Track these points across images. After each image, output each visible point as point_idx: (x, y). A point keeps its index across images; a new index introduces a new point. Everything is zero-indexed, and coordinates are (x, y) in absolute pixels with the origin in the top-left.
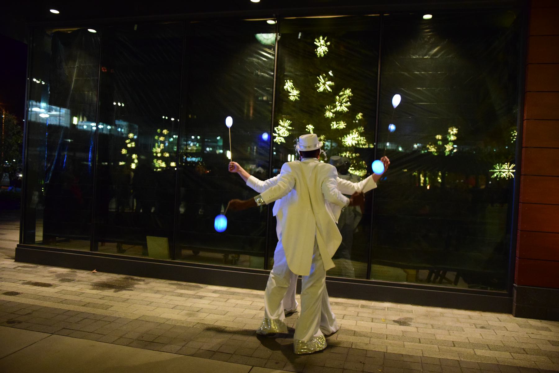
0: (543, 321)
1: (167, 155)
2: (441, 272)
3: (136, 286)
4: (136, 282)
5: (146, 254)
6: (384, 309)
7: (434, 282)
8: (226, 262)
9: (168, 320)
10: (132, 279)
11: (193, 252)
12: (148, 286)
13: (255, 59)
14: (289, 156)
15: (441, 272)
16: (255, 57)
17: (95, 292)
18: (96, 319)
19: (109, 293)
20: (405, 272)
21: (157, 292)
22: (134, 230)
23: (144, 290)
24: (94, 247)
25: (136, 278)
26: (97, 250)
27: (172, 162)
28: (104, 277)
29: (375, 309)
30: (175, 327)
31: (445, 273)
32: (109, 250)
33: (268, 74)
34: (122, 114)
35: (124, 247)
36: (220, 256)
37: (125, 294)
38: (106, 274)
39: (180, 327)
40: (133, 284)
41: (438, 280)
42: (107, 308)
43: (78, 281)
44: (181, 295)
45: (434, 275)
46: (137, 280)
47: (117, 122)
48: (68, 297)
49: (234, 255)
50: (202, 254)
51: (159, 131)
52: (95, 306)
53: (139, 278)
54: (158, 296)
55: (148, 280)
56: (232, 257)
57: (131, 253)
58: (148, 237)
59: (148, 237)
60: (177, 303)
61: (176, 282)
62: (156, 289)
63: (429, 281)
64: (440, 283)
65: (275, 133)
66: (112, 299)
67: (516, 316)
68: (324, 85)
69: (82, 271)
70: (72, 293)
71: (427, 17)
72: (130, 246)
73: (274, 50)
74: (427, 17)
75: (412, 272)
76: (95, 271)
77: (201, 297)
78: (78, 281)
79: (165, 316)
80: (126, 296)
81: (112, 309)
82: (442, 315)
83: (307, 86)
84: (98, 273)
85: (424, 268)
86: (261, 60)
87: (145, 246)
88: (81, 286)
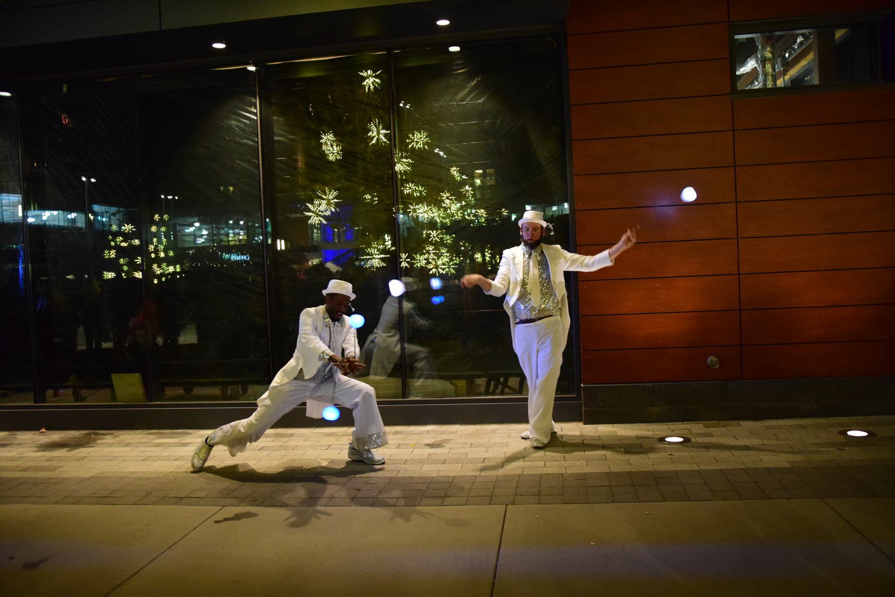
0: (615, 425)
1: (171, 254)
2: (502, 380)
3: (99, 442)
4: (101, 437)
5: (114, 399)
6: (428, 432)
7: (494, 394)
8: (225, 398)
9: (132, 473)
10: (95, 434)
11: (184, 389)
12: (118, 439)
13: (234, 123)
14: (283, 248)
15: (502, 380)
16: (233, 119)
17: (40, 454)
18: (36, 482)
19: (62, 453)
20: (451, 383)
21: (128, 444)
22: (97, 371)
23: (110, 445)
24: (40, 397)
25: (102, 432)
26: (45, 402)
27: (528, 204)
28: (56, 436)
29: (411, 433)
30: (140, 479)
31: (506, 380)
32: (65, 399)
33: (251, 140)
34: (102, 195)
35: (84, 392)
36: (217, 391)
37: (82, 452)
38: (59, 432)
39: (148, 479)
40: (95, 440)
41: (499, 390)
42: (53, 469)
43: (19, 444)
44: (159, 445)
45: (493, 383)
46: (103, 434)
47: (96, 208)
48: (9, 464)
49: (232, 387)
50: (197, 391)
51: (157, 217)
52: (37, 469)
53: (106, 432)
54: (128, 449)
55: (116, 433)
56: (232, 389)
57: (95, 399)
58: (114, 376)
59: (114, 376)
60: (149, 454)
61: (156, 431)
62: (127, 441)
63: (487, 393)
64: (502, 393)
65: (310, 211)
66: (60, 459)
67: (585, 424)
68: (377, 134)
69: (26, 432)
70: (12, 459)
71: (454, 49)
72: (91, 392)
73: (256, 108)
74: (454, 49)
75: (462, 383)
76: (43, 430)
77: (185, 445)
78: (19, 444)
79: (131, 469)
80: (83, 455)
81: (61, 469)
82: (494, 431)
83: (354, 137)
84: (49, 433)
85: (479, 377)
86: (242, 122)
87: (111, 387)
88: (21, 450)
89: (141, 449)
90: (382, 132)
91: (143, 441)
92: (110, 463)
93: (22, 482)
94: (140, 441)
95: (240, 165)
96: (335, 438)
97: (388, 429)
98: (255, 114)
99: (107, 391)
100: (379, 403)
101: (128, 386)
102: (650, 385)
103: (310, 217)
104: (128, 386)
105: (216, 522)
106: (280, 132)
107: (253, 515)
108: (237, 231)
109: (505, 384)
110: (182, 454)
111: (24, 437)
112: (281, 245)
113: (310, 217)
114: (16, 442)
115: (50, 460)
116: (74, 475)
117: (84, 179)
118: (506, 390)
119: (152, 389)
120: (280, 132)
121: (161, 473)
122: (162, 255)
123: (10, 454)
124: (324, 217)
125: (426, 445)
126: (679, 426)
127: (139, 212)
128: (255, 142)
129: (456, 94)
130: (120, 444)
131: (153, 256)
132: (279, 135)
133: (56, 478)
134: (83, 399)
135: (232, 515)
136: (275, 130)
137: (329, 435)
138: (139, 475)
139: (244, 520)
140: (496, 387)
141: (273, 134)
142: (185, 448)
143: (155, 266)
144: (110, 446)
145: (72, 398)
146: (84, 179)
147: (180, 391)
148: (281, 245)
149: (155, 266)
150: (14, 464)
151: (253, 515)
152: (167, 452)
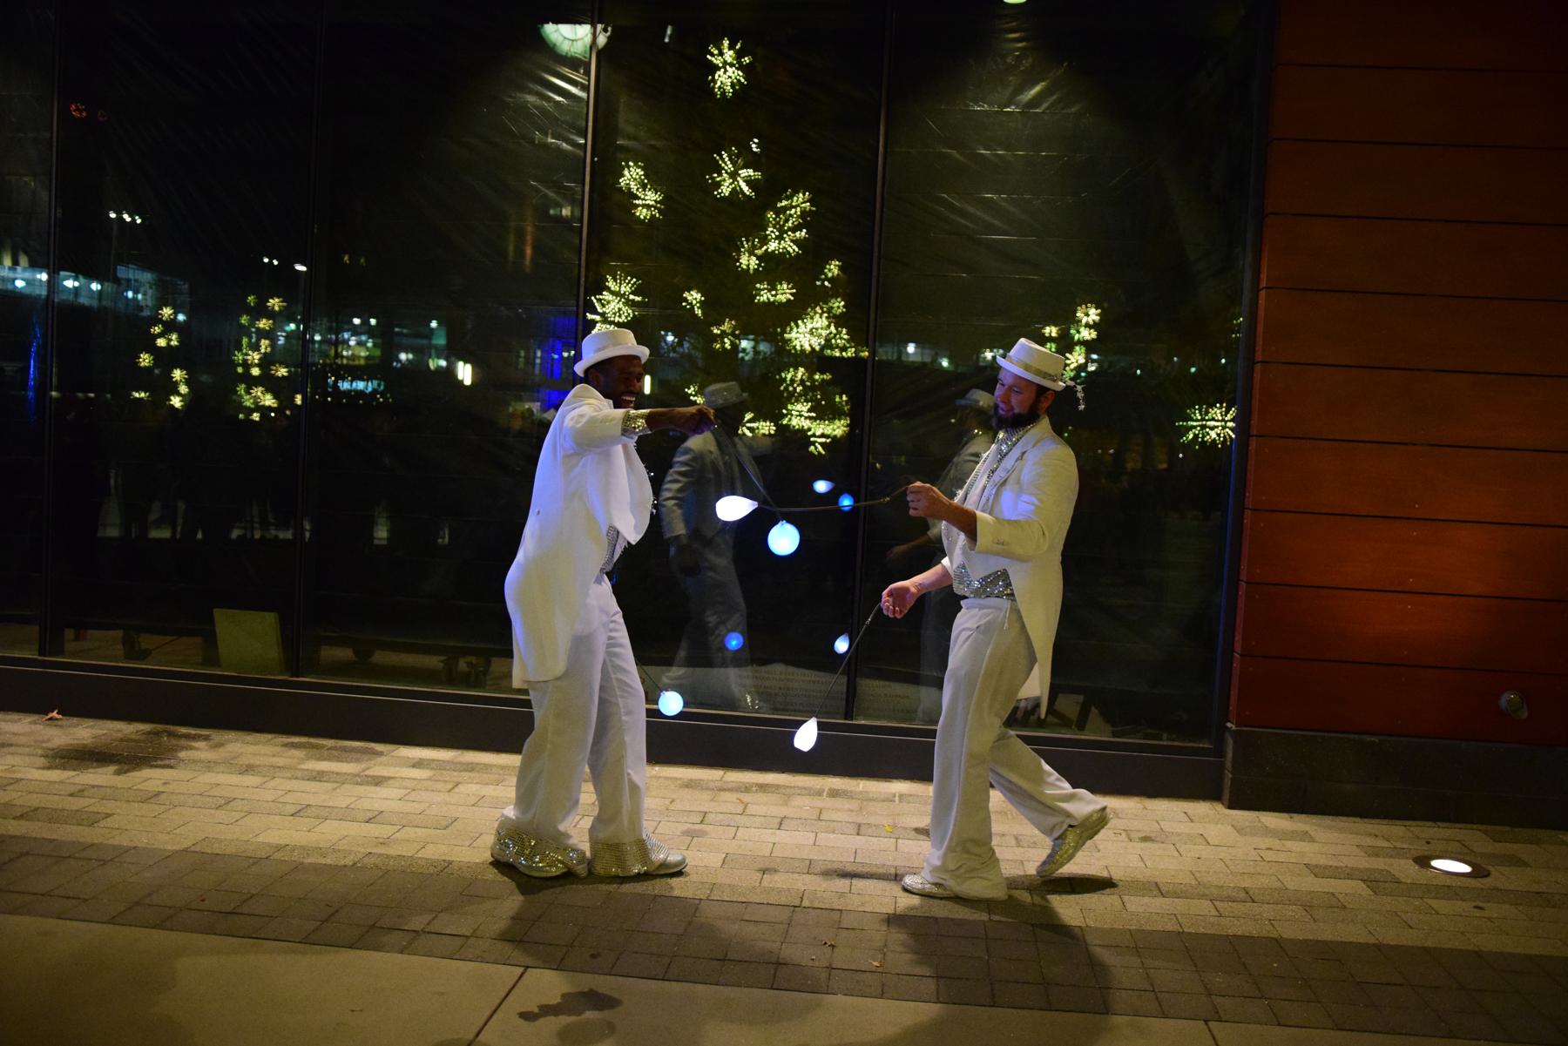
3: (182, 754)
5: (212, 659)
8: (452, 678)
9: (279, 848)
10: (171, 734)
11: (355, 652)
12: (220, 754)
13: (531, 99)
16: (531, 92)
17: (55, 775)
18: (59, 854)
19: (101, 776)
21: (249, 769)
22: (179, 594)
23: (209, 766)
24: (51, 643)
25: (183, 730)
26: (61, 653)
28: (85, 732)
29: (867, 799)
30: (299, 867)
32: (99, 650)
34: (136, 247)
35: (146, 641)
36: (433, 661)
37: (149, 778)
38: (91, 722)
40: (174, 750)
42: (93, 820)
44: (318, 777)
46: (187, 736)
49: (473, 659)
50: (381, 657)
52: (56, 817)
53: (193, 731)
54: (251, 780)
55: (217, 736)
56: (469, 664)
57: (169, 657)
58: (218, 614)
59: (218, 614)
61: (303, 740)
62: (244, 760)
65: (595, 312)
67: (1231, 807)
69: (15, 716)
73: (587, 73)
76: (55, 714)
77: (378, 781)
81: (108, 822)
83: (684, 180)
86: (550, 99)
87: (211, 639)
88: (10, 760)
89: (281, 783)
90: (744, 173)
91: (280, 761)
95: (538, 191)
98: (585, 88)
101: (248, 638)
102: (1376, 739)
104: (248, 638)
105: (526, 1016)
106: (630, 129)
108: (363, 338)
110: (377, 806)
111: (14, 728)
112: (465, 373)
115: (80, 793)
116: (143, 841)
117: (113, 215)
120: (630, 129)
122: (255, 372)
126: (1474, 836)
127: (218, 285)
128: (579, 145)
130: (231, 765)
131: (240, 370)
132: (629, 138)
133: (99, 846)
134: (143, 655)
136: (621, 124)
137: (690, 785)
138: (296, 856)
142: (382, 791)
143: (241, 389)
145: (119, 649)
146: (113, 215)
147: (344, 654)
148: (465, 373)
152: (343, 797)
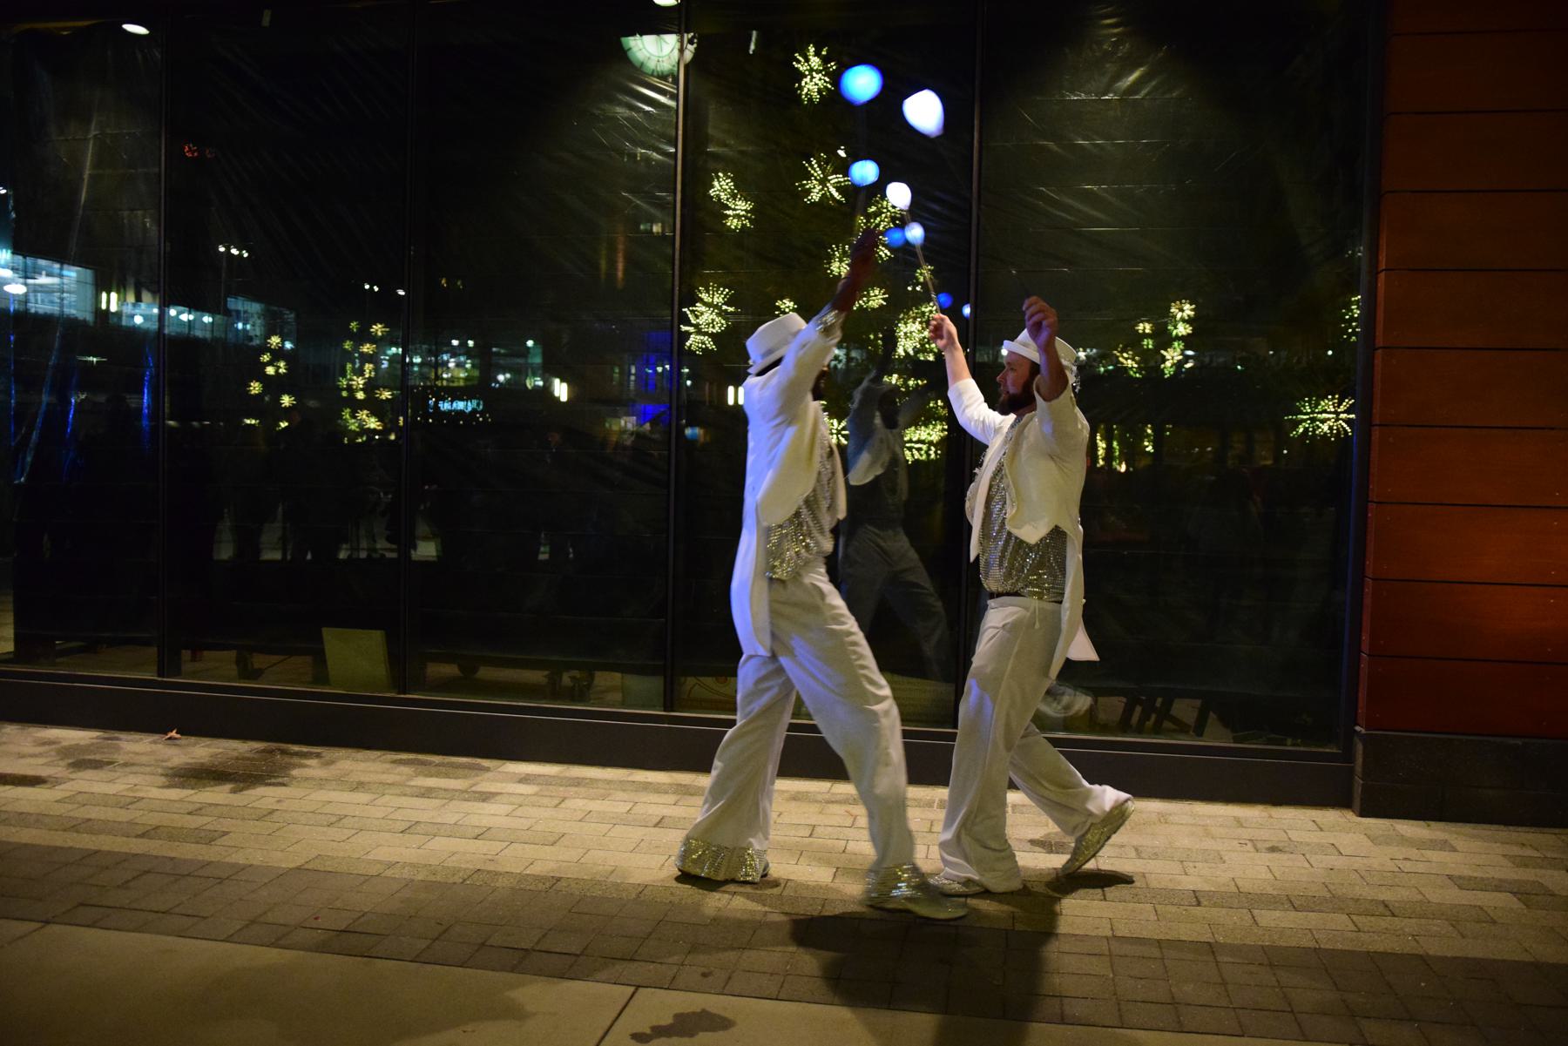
3: (295, 772)
4: (295, 760)
5: (321, 677)
7: (1140, 730)
8: (555, 693)
9: (391, 865)
10: (283, 752)
12: (333, 771)
16: (621, 104)
17: (175, 794)
18: (178, 872)
19: (218, 795)
21: (359, 786)
23: (321, 783)
24: (168, 665)
25: (296, 748)
26: (178, 674)
28: (202, 751)
31: (1168, 704)
32: (215, 670)
34: (247, 280)
35: (259, 661)
36: (537, 676)
37: (264, 796)
38: (207, 741)
41: (1150, 723)
42: (209, 838)
43: (125, 765)
44: (427, 793)
45: (1138, 709)
49: (576, 673)
50: (486, 673)
52: (174, 834)
53: (305, 749)
54: (362, 797)
57: (281, 677)
60: (415, 816)
61: (412, 756)
62: (355, 778)
64: (1157, 730)
69: (137, 736)
76: (173, 734)
77: (486, 797)
78: (125, 765)
81: (225, 840)
82: (1163, 818)
84: (185, 740)
87: (319, 657)
88: (132, 779)
89: (390, 800)
91: (389, 778)
92: (332, 831)
93: (147, 868)
94: (384, 778)
96: (814, 808)
97: (916, 792)
98: (674, 97)
99: (302, 663)
100: (906, 734)
102: (1519, 742)
103: (688, 334)
107: (720, 1023)
108: (462, 359)
109: (1165, 714)
110: (485, 822)
112: (561, 390)
113: (688, 334)
114: (121, 759)
116: (257, 858)
118: (1167, 724)
119: (403, 673)
121: (455, 871)
122: (360, 395)
123: (110, 789)
124: (712, 335)
125: (1032, 842)
129: (1118, 76)
130: (341, 782)
131: (344, 394)
134: (256, 675)
135: (666, 1020)
136: (711, 131)
139: (703, 1037)
140: (1145, 717)
141: (707, 140)
142: (489, 808)
143: (346, 414)
144: (321, 787)
146: (222, 249)
147: (450, 670)
149: (346, 414)
150: (123, 816)
151: (720, 1023)
152: (452, 813)
